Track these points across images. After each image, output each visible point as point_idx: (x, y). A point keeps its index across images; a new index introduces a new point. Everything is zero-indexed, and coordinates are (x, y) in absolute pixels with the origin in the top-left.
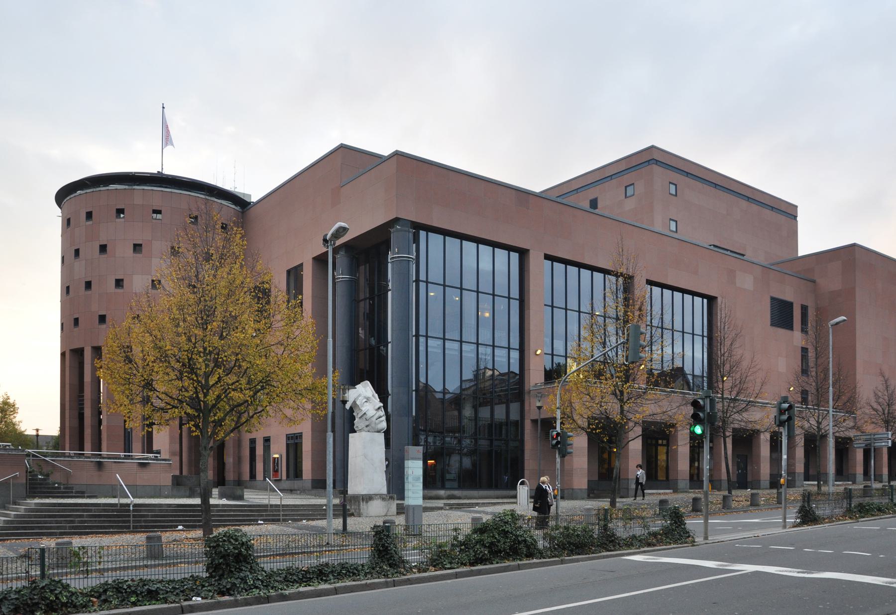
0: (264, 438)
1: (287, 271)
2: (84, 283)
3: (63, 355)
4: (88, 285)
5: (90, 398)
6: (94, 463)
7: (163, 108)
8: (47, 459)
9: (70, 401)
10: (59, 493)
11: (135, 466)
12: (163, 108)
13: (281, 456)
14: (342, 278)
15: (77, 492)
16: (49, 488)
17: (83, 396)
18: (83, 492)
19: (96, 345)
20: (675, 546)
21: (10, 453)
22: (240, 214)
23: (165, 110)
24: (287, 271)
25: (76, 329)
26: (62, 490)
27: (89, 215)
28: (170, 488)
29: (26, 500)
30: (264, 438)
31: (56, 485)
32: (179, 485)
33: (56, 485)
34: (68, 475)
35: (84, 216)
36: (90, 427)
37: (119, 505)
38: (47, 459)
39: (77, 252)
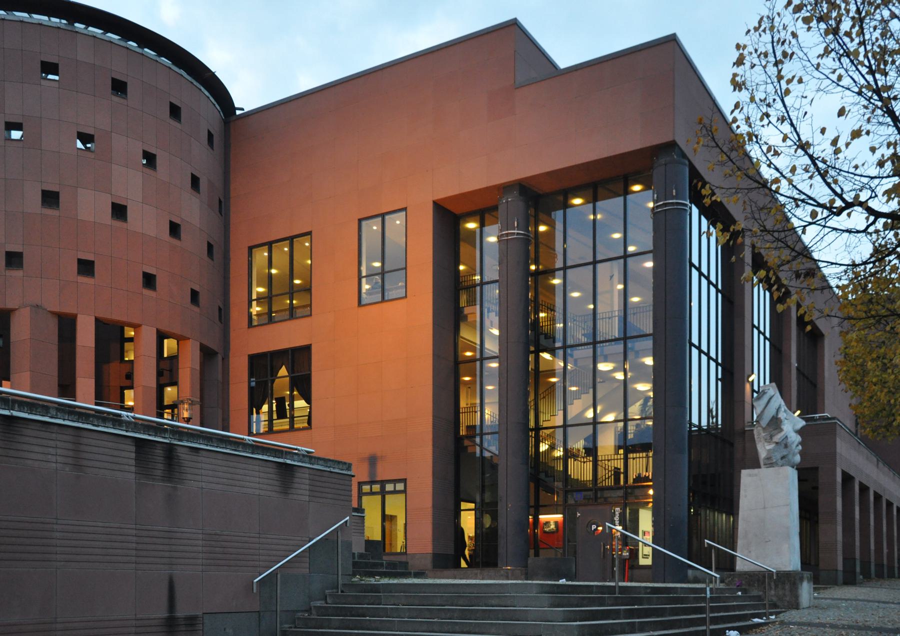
14: (518, 234)
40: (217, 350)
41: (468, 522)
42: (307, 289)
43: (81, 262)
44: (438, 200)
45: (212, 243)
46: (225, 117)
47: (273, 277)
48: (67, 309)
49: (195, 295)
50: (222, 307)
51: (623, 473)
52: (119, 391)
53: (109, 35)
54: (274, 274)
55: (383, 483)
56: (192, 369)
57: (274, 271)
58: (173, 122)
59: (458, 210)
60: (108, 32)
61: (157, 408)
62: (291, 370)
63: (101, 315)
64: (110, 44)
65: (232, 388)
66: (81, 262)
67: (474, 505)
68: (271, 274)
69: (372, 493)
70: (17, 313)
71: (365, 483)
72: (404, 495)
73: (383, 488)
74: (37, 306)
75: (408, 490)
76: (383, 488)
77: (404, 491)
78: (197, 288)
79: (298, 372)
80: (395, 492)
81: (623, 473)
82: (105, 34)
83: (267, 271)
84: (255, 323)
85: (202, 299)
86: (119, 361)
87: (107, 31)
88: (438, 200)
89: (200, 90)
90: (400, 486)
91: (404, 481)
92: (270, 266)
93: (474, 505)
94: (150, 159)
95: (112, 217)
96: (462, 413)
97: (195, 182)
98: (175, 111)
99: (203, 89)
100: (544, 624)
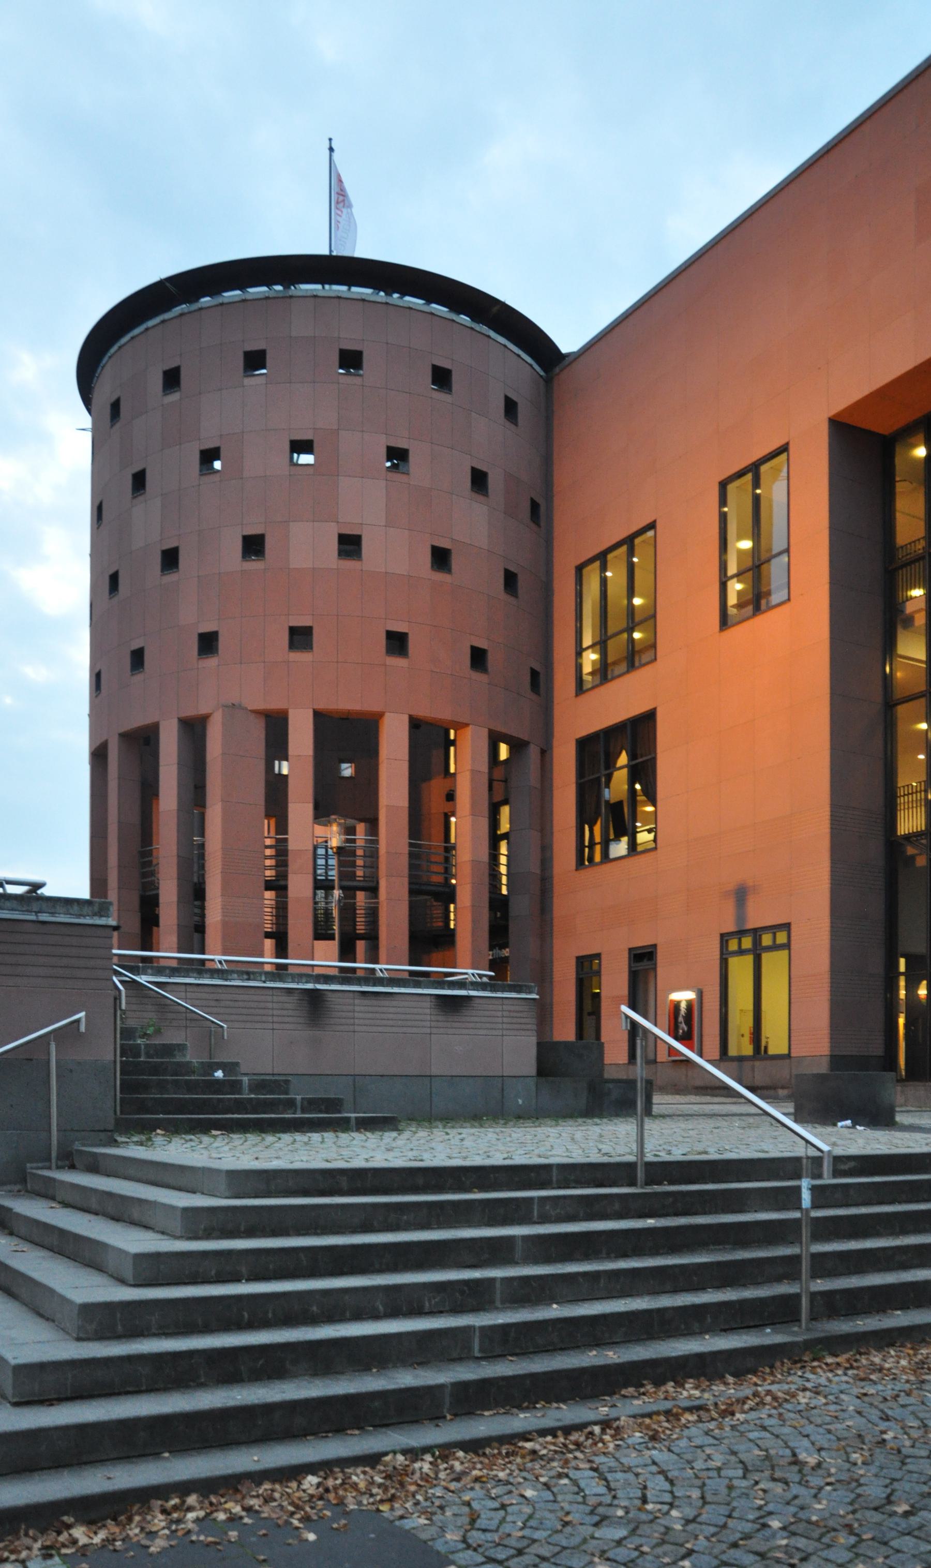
0: (630, 950)
1: (720, 483)
2: (160, 553)
3: (99, 756)
4: (170, 559)
5: (175, 852)
6: (294, 998)
7: (331, 149)
8: (142, 979)
9: (119, 866)
10: (240, 1106)
11: (427, 1007)
12: (331, 149)
13: (700, 994)
15: (311, 1104)
16: (191, 1087)
17: (150, 853)
18: (333, 1104)
19: (189, 712)
20: (118, 1098)
21: (44, 917)
22: (542, 383)
23: (335, 155)
24: (720, 483)
25: (139, 677)
26: (246, 1095)
27: (172, 379)
28: (531, 1083)
29: (115, 1143)
30: (630, 950)
31: (219, 1074)
32: (547, 1075)
33: (219, 1074)
34: (211, 1035)
35: (157, 381)
36: (175, 927)
37: (640, 1174)
38: (142, 979)
39: (139, 481)
40: (526, 739)
41: (888, 995)
42: (650, 618)
43: (293, 631)
44: (834, 416)
45: (512, 569)
46: (545, 371)
47: (636, 611)
48: (274, 704)
49: (478, 658)
50: (537, 667)
51: (588, 847)
52: (442, 820)
53: (407, 298)
54: (639, 606)
55: (756, 933)
56: (473, 772)
57: (637, 601)
58: (442, 396)
59: (884, 426)
60: (432, 302)
61: (411, 837)
62: (632, 756)
63: (322, 705)
64: (430, 316)
65: (557, 794)
66: (293, 631)
67: (358, 942)
68: (633, 605)
69: (741, 952)
70: (211, 718)
71: (731, 934)
72: (786, 952)
73: (757, 942)
74: (234, 705)
75: (793, 943)
76: (757, 942)
77: (787, 946)
78: (482, 644)
79: (642, 757)
80: (775, 947)
81: (588, 847)
82: (378, 294)
83: (625, 602)
84: (587, 686)
85: (493, 660)
86: (443, 776)
87: (429, 301)
88: (839, 414)
89: (489, 337)
90: (782, 938)
91: (787, 927)
92: (631, 593)
93: (358, 942)
94: (398, 455)
95: (432, 566)
96: (901, 796)
97: (479, 480)
98: (442, 378)
99: (492, 334)
100: (543, 1199)
